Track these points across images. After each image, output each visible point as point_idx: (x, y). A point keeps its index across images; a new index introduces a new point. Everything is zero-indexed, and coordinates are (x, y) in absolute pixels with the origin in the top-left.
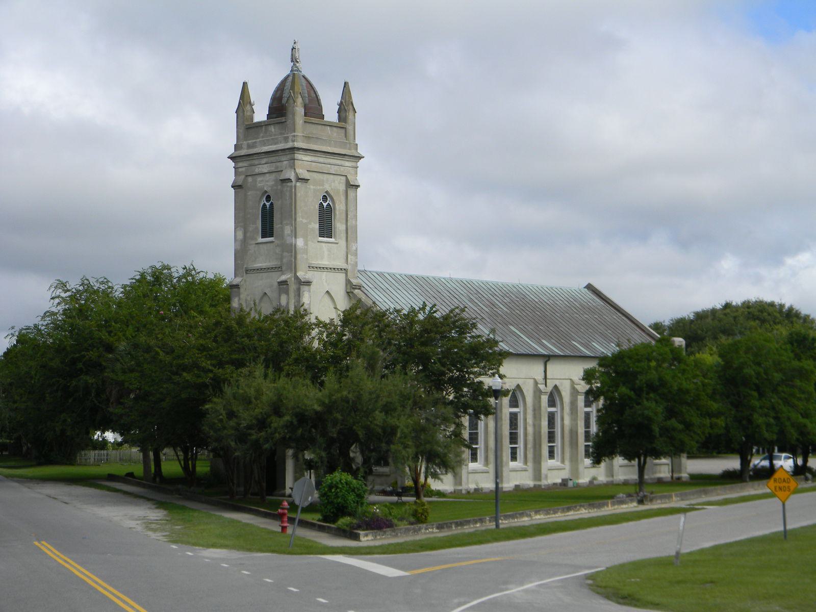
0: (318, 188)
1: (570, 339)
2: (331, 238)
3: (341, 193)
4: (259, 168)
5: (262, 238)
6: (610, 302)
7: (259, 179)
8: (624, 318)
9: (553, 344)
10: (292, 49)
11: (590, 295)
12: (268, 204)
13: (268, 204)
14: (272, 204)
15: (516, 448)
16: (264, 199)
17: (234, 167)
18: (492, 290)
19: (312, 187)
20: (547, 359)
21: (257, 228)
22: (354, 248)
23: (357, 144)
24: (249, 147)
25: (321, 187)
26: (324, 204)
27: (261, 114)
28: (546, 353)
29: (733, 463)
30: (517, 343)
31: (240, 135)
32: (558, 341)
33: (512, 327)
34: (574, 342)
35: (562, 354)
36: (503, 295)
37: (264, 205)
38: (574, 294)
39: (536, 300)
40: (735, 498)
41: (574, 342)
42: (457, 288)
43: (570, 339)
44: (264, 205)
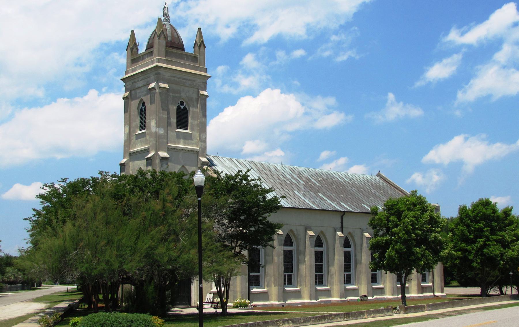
0: (177, 95)
1: (361, 203)
2: (187, 130)
3: (194, 100)
4: (138, 84)
5: (140, 131)
6: (392, 184)
7: (138, 91)
8: (401, 193)
9: (348, 205)
10: (164, 8)
11: (378, 179)
12: (143, 108)
13: (143, 108)
14: (145, 108)
15: (322, 275)
16: (141, 105)
17: (124, 86)
18: (311, 173)
19: (171, 94)
20: (343, 214)
21: (137, 124)
22: (204, 137)
23: (206, 68)
24: (133, 71)
25: (179, 95)
26: (181, 107)
27: (142, 49)
28: (342, 210)
29: (477, 290)
30: (322, 204)
31: (128, 64)
32: (352, 203)
33: (320, 194)
34: (364, 205)
35: (353, 211)
36: (317, 176)
37: (142, 108)
38: (368, 179)
39: (341, 180)
40: (507, 304)
41: (364, 205)
42: (285, 171)
43: (361, 203)
44: (142, 108)
